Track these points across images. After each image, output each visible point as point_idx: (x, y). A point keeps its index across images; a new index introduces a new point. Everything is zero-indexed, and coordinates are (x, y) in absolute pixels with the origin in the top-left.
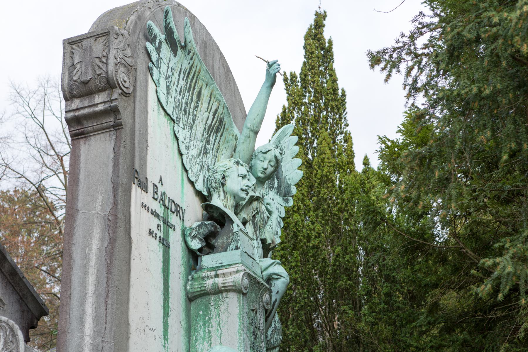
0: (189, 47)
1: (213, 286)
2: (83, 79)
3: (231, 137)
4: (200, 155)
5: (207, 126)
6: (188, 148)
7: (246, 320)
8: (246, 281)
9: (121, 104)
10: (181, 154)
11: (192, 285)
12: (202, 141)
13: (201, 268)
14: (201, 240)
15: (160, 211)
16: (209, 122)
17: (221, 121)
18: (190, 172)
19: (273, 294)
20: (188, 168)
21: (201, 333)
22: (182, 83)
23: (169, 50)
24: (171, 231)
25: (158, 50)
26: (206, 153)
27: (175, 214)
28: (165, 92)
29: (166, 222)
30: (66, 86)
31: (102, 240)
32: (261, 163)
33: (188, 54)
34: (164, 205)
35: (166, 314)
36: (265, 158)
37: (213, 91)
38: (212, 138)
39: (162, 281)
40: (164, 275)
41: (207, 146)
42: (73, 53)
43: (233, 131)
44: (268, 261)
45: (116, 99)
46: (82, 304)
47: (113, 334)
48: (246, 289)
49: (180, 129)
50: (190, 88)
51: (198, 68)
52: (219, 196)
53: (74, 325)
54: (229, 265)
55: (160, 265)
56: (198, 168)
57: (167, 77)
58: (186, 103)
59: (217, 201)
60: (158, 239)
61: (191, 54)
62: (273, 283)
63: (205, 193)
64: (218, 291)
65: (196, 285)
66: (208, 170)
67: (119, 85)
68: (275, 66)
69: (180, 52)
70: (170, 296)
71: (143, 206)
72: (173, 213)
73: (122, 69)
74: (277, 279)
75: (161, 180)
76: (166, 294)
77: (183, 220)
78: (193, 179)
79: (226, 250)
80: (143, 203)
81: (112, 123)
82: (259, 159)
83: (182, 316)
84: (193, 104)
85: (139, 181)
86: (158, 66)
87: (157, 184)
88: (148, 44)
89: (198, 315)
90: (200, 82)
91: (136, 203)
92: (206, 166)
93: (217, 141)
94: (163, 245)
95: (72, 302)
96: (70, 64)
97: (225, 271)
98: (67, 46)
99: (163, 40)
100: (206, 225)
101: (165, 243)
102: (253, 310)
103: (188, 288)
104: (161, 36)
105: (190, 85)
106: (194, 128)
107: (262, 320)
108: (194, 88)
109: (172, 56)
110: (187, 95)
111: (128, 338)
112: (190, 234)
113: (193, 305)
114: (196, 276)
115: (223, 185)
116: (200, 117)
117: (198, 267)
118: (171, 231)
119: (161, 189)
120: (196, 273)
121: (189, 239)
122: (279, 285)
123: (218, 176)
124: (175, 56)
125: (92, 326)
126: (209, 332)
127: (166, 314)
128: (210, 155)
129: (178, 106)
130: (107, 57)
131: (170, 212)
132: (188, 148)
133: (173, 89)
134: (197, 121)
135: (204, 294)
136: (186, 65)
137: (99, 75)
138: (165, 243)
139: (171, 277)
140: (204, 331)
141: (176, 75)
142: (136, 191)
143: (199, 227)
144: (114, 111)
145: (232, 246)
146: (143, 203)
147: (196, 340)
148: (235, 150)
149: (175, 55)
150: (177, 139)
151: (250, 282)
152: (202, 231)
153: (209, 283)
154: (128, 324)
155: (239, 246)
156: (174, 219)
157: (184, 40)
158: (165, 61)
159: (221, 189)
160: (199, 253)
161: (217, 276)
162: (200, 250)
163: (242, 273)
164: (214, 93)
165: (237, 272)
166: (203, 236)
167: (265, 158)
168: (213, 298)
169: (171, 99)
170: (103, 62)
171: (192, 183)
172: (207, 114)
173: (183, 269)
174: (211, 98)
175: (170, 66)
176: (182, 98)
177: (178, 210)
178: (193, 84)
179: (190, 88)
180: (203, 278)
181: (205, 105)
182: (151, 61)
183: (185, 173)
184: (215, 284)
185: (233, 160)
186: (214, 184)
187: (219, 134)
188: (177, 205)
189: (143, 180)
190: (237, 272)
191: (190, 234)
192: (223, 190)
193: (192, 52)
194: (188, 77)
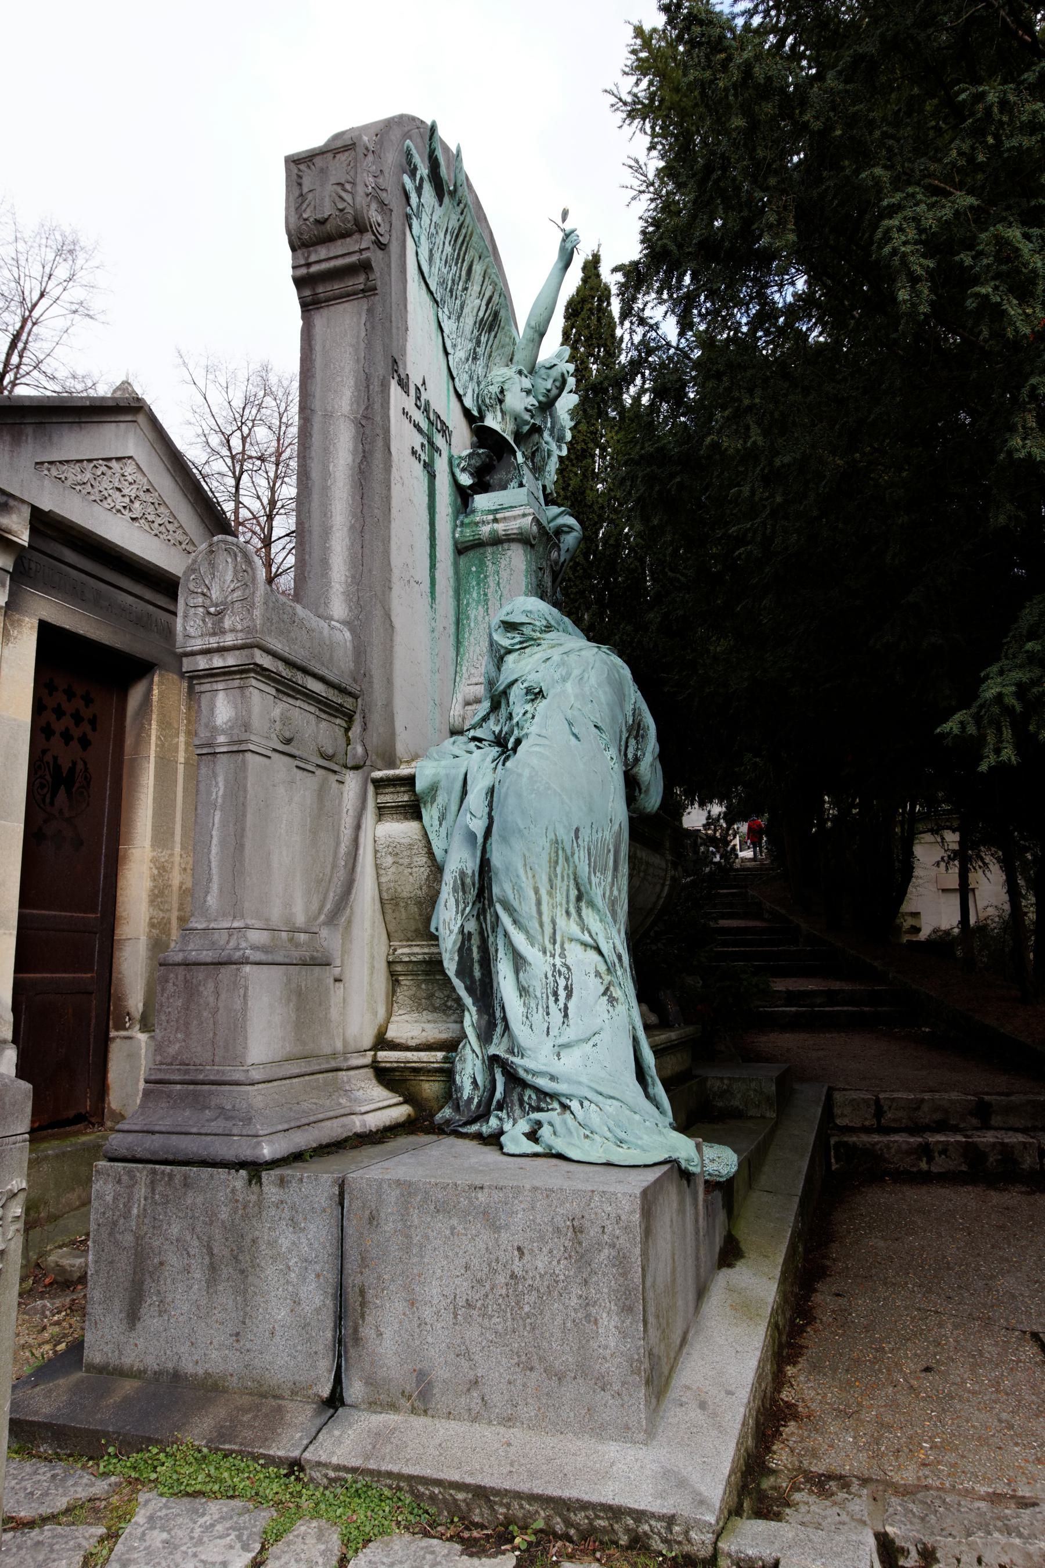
0: (459, 193)
1: (490, 533)
2: (319, 216)
3: (507, 339)
4: (468, 360)
5: (479, 319)
6: (454, 346)
7: (534, 579)
8: (535, 528)
9: (376, 257)
10: (447, 354)
11: (462, 532)
12: (471, 340)
13: (473, 511)
14: (471, 474)
15: (424, 425)
16: (481, 314)
17: (496, 314)
18: (457, 380)
19: (562, 552)
20: (455, 374)
21: (475, 595)
22: (448, 249)
23: (433, 194)
24: (436, 455)
25: (419, 190)
26: (475, 359)
28: (427, 258)
29: (431, 443)
30: (291, 226)
32: (544, 383)
33: (458, 205)
34: (429, 419)
35: (433, 566)
36: (548, 376)
37: (487, 267)
38: (483, 339)
39: (428, 521)
41: (478, 349)
42: (300, 177)
43: (510, 331)
44: (555, 510)
45: (368, 248)
48: (534, 538)
49: (446, 318)
50: (457, 259)
51: (470, 229)
52: (495, 418)
54: (512, 507)
55: (426, 499)
56: (466, 377)
57: (430, 236)
58: (453, 281)
59: (492, 421)
61: (462, 205)
62: (563, 537)
63: (476, 413)
64: (497, 541)
65: (468, 532)
66: (479, 383)
67: (371, 227)
68: (572, 237)
69: (446, 199)
71: (405, 413)
73: (374, 206)
74: (568, 532)
75: (424, 383)
78: (461, 392)
79: (505, 488)
81: (362, 287)
82: (540, 377)
83: (451, 572)
84: (461, 284)
85: (399, 376)
86: (419, 217)
87: (420, 386)
88: (406, 179)
89: (470, 572)
90: (472, 253)
91: (396, 406)
92: (475, 377)
93: (490, 343)
96: (297, 194)
97: (507, 514)
98: (292, 166)
99: (426, 177)
100: (478, 454)
101: (429, 467)
102: (541, 569)
103: (457, 535)
104: (423, 171)
105: (459, 254)
106: (462, 319)
107: (550, 584)
108: (463, 260)
109: (437, 205)
110: (454, 268)
112: (459, 465)
113: (463, 560)
114: (467, 521)
115: (501, 402)
116: (470, 306)
117: (468, 510)
119: (424, 396)
120: (466, 516)
121: (457, 471)
122: (570, 540)
123: (495, 389)
124: (441, 205)
126: (485, 595)
127: (433, 566)
128: (481, 362)
129: (442, 283)
130: (354, 184)
132: (454, 346)
133: (437, 256)
134: (466, 310)
135: (478, 544)
136: (454, 223)
137: (341, 210)
138: (429, 467)
139: (437, 517)
140: (479, 593)
141: (442, 235)
142: (394, 388)
143: (470, 456)
144: (365, 267)
145: (514, 484)
147: (468, 604)
148: (511, 360)
149: (441, 202)
150: (442, 331)
151: (539, 529)
152: (473, 462)
153: (485, 530)
155: (524, 482)
156: (439, 441)
157: (453, 182)
158: (428, 209)
159: (498, 407)
161: (495, 520)
162: (471, 487)
163: (530, 518)
164: (489, 271)
165: (524, 515)
167: (548, 376)
168: (490, 550)
169: (435, 270)
170: (346, 191)
171: (459, 397)
172: (478, 301)
173: (450, 510)
174: (484, 277)
175: (434, 220)
176: (448, 273)
177: (444, 430)
178: (462, 253)
179: (459, 259)
180: (477, 524)
181: (476, 288)
182: (410, 205)
183: (451, 381)
184: (493, 532)
185: (514, 368)
186: (487, 401)
187: (493, 334)
188: (443, 423)
189: (403, 376)
190: (524, 515)
191: (459, 465)
192: (501, 409)
193: (464, 202)
194: (456, 241)
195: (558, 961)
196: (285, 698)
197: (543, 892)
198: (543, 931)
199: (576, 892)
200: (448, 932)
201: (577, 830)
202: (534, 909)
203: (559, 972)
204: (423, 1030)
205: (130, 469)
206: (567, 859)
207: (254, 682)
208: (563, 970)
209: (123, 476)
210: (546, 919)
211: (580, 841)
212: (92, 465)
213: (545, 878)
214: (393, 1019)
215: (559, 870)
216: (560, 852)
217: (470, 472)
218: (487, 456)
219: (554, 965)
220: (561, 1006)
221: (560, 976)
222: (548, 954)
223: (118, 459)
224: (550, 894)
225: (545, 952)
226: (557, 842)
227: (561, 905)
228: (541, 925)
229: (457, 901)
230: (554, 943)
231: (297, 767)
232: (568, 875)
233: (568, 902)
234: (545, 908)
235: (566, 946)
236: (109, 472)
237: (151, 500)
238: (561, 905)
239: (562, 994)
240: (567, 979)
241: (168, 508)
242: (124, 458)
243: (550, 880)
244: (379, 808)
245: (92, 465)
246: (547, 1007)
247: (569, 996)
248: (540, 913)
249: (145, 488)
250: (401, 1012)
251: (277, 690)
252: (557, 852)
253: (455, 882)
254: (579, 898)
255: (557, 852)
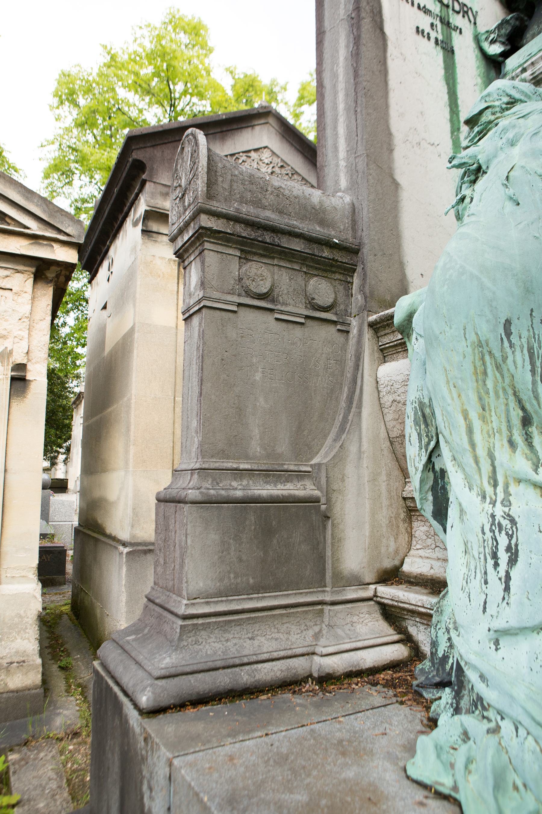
14: (503, 43)
24: (455, 35)
27: (461, 14)
29: (446, 23)
31: (347, 46)
40: (448, 84)
46: (335, 128)
47: (364, 143)
53: (330, 154)
60: (433, 40)
70: (460, 109)
72: (458, 13)
76: (453, 106)
77: (475, 24)
80: (418, 28)
94: (443, 48)
95: (326, 132)
111: (391, 151)
118: (455, 35)
121: (486, 46)
125: (345, 146)
131: (451, 12)
146: (418, 28)
154: (390, 134)
156: (457, 20)
160: (501, 59)
166: (506, 38)
191: (486, 39)
195: (499, 511)
196: (255, 258)
197: (474, 415)
198: (479, 469)
199: (521, 414)
200: (414, 470)
201: (508, 323)
202: (465, 439)
203: (500, 525)
204: (432, 568)
205: (266, 156)
206: (498, 367)
207: (207, 245)
208: (505, 523)
209: (261, 160)
210: (481, 452)
211: (514, 339)
212: (234, 158)
213: (473, 397)
214: (412, 552)
215: (490, 384)
216: (487, 358)
217: (500, 42)
218: (517, 19)
219: (493, 516)
220: (502, 574)
221: (500, 532)
222: (488, 500)
223: (256, 150)
224: (483, 419)
225: (484, 497)
226: (480, 345)
227: (500, 431)
228: (477, 462)
229: (419, 435)
230: (495, 485)
231: (277, 319)
232: (504, 389)
233: (510, 428)
234: (478, 437)
235: (512, 489)
236: (249, 160)
237: (285, 172)
238: (500, 431)
239: (504, 557)
240: (510, 537)
241: (300, 175)
242: (261, 148)
243: (480, 399)
244: (382, 350)
245: (234, 158)
246: (486, 573)
247: (513, 561)
248: (473, 445)
249: (279, 165)
250: (418, 546)
251: (242, 251)
252: (483, 359)
253: (416, 414)
254: (526, 421)
255: (483, 359)
